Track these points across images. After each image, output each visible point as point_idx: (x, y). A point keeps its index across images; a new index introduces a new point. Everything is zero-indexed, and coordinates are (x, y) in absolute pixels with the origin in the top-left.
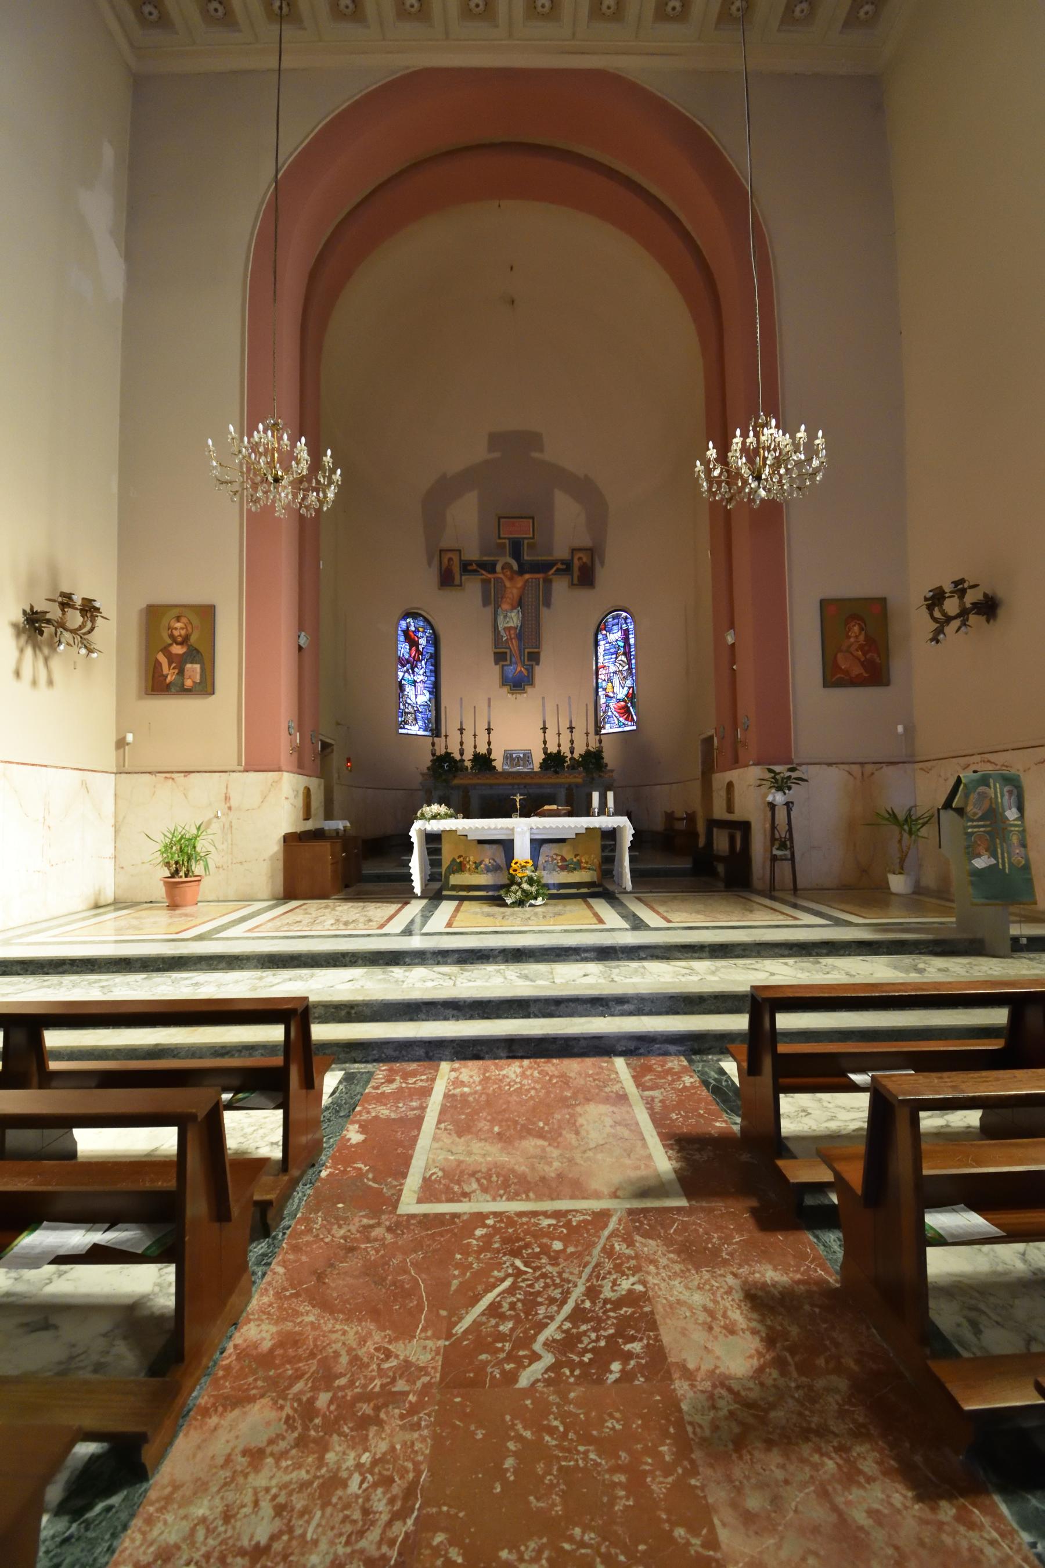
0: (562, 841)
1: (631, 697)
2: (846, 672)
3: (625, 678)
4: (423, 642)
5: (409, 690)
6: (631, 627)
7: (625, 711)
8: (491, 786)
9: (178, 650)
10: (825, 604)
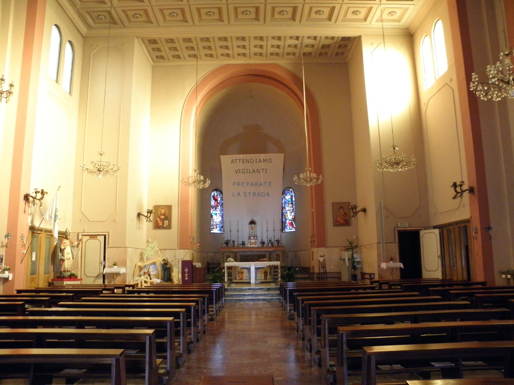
0: (263, 268)
1: (294, 219)
2: (339, 222)
3: (291, 212)
4: (219, 199)
5: (214, 217)
6: (293, 194)
7: (291, 224)
8: (244, 252)
9: (162, 217)
10: (333, 204)
